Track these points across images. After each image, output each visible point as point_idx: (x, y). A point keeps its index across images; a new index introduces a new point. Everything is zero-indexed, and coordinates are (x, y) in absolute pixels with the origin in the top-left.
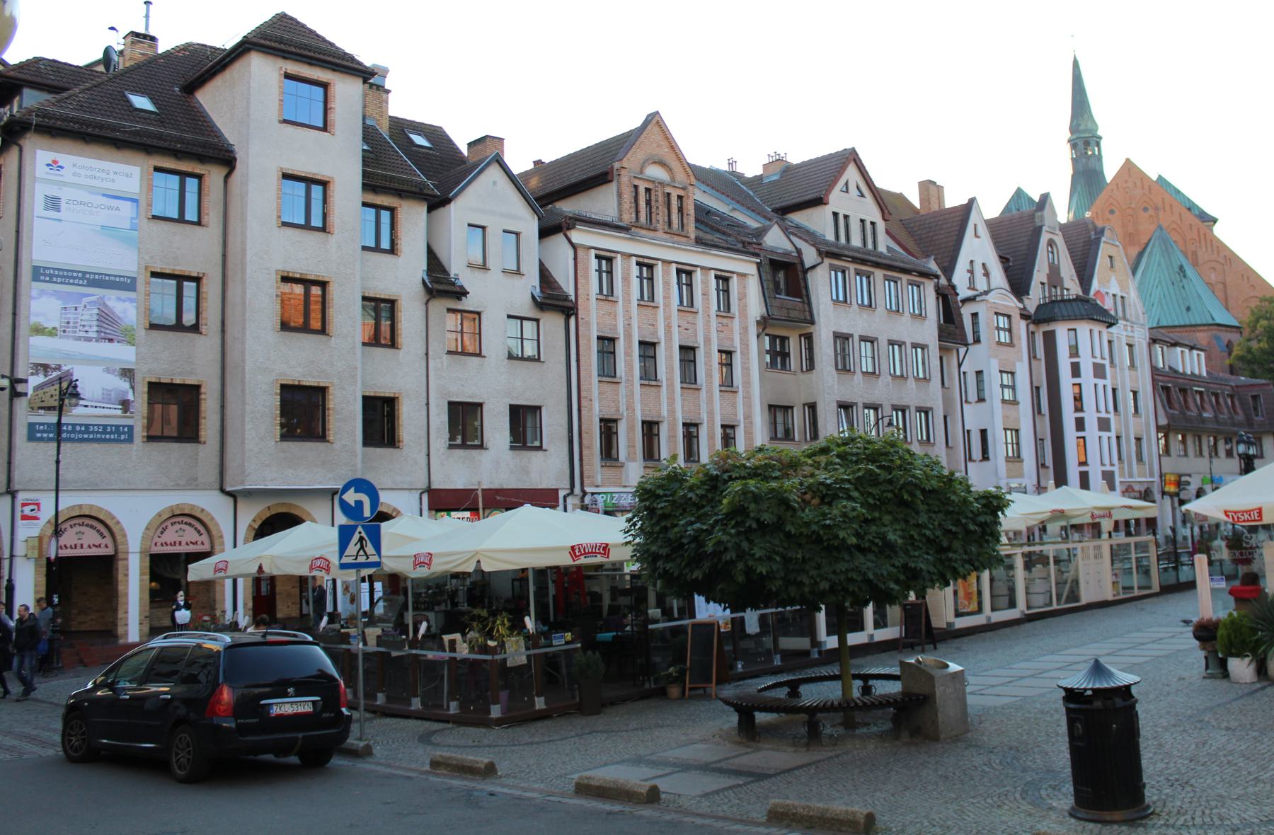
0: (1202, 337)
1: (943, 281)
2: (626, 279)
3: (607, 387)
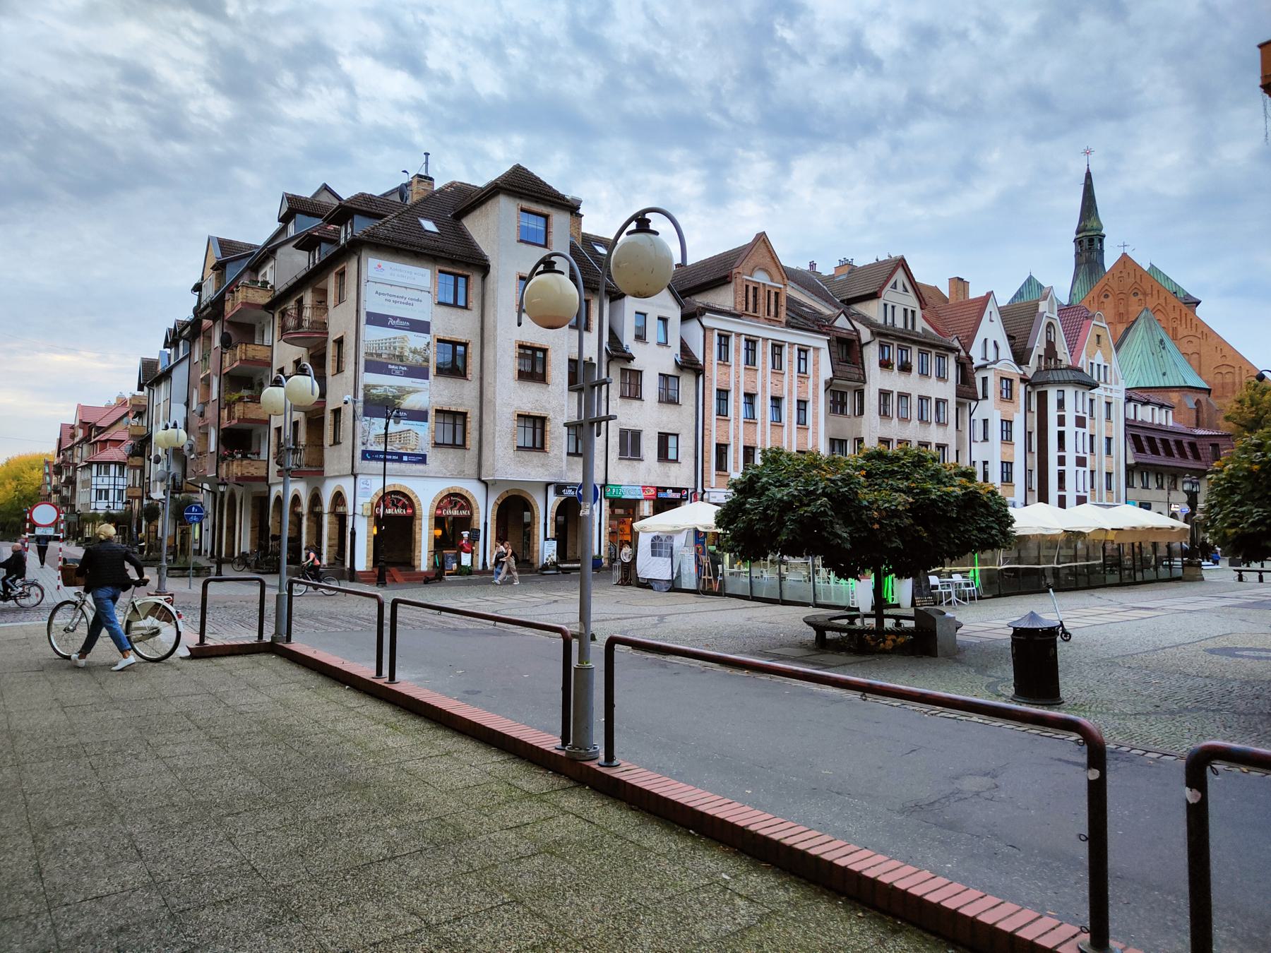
0: (1174, 397)
1: (963, 354)
2: (737, 350)
3: (721, 423)
